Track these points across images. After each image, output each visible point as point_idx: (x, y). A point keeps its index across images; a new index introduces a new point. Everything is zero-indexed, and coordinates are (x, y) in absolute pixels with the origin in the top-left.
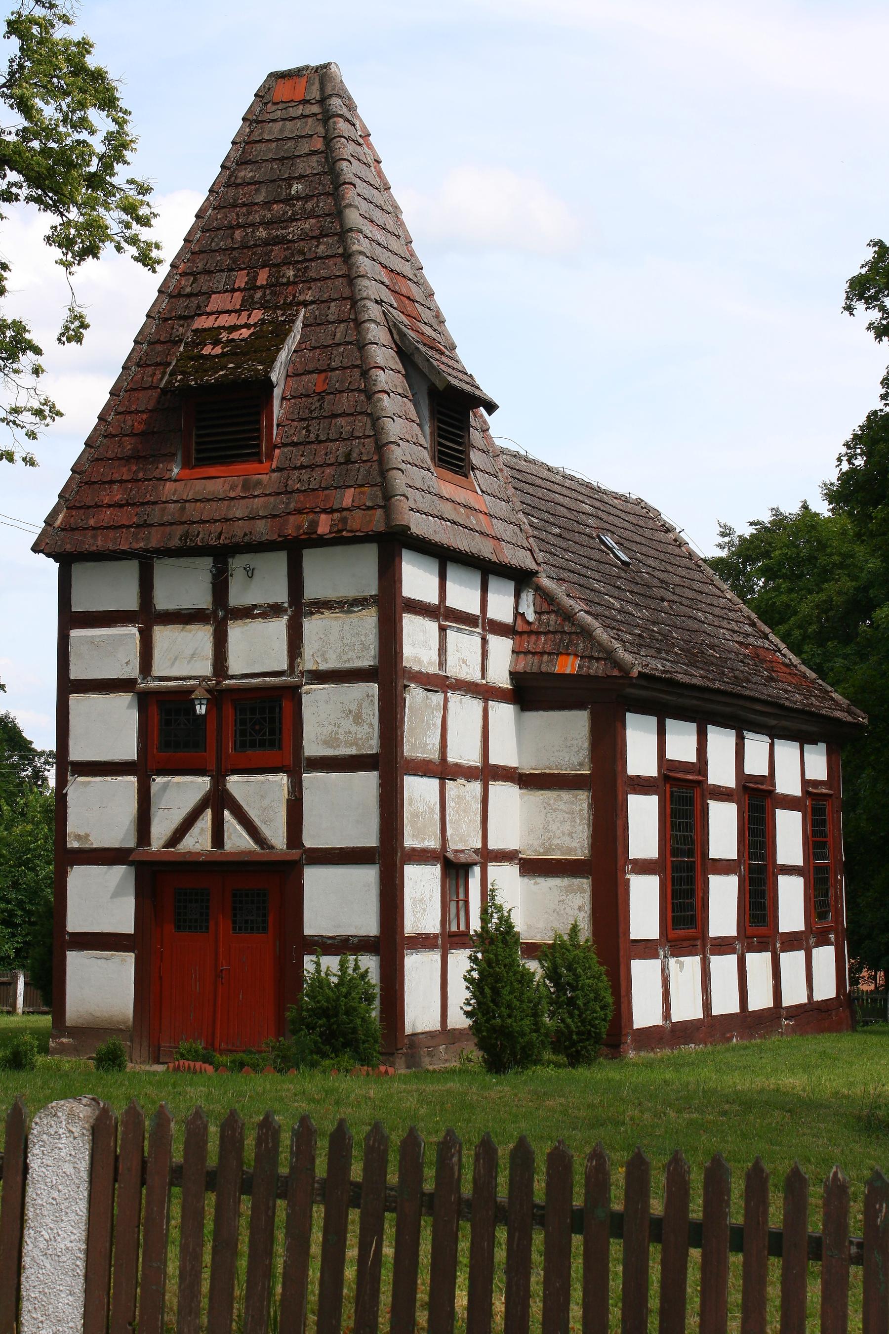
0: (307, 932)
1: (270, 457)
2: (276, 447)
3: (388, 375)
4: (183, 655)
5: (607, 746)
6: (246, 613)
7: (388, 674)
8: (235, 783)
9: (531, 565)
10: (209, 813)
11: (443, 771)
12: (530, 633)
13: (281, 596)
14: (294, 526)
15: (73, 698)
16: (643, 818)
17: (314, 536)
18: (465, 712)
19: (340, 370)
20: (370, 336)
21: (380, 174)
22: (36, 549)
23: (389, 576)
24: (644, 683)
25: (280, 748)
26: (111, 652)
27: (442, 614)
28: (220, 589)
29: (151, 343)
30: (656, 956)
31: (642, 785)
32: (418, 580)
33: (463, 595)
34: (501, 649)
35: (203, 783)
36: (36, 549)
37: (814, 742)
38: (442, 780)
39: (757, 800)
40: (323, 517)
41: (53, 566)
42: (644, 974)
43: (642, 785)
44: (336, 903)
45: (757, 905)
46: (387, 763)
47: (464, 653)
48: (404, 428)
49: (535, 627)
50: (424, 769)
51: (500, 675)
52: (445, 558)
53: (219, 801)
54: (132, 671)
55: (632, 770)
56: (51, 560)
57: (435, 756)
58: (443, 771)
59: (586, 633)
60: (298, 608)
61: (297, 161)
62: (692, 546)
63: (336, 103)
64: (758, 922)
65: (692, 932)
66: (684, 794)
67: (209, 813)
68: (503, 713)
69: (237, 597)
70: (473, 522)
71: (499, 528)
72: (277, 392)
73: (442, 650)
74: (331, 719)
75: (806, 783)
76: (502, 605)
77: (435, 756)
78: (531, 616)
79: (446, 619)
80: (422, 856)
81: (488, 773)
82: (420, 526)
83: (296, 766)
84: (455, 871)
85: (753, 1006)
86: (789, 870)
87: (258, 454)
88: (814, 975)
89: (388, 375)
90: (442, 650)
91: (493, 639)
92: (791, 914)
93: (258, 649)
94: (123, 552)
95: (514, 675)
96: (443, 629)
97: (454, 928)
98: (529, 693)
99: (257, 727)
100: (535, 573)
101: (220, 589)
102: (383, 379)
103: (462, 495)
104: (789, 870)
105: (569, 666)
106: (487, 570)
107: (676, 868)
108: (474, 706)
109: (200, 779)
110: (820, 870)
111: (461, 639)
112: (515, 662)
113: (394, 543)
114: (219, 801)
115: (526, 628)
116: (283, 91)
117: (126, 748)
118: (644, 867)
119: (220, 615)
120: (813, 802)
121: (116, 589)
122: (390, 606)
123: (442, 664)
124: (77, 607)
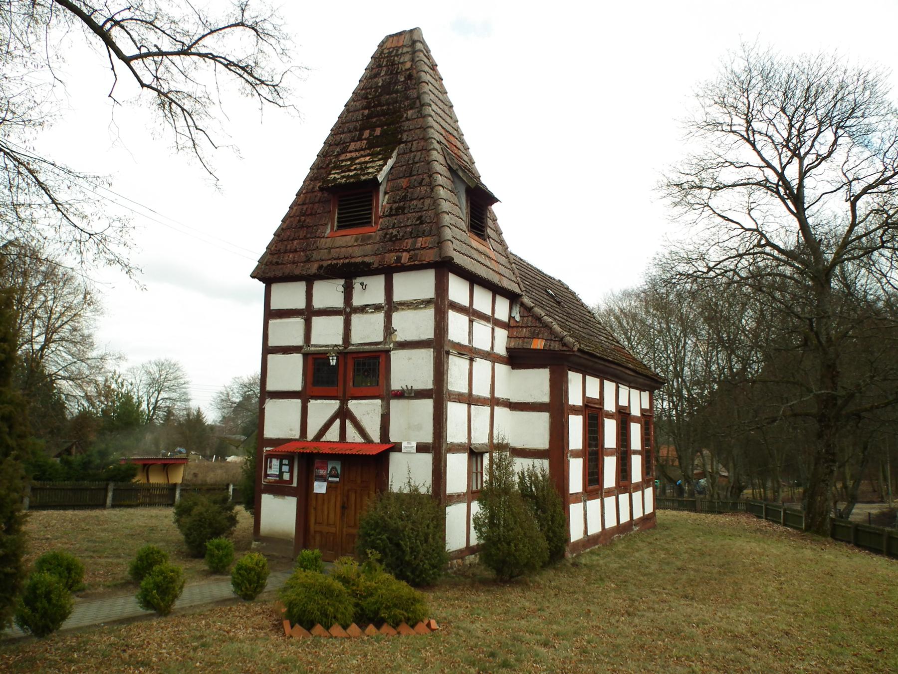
1: (376, 223)
2: (380, 217)
3: (442, 178)
4: (327, 333)
5: (558, 388)
6: (363, 309)
7: (439, 346)
8: (353, 405)
9: (517, 290)
10: (338, 421)
11: (470, 400)
12: (518, 327)
13: (380, 299)
14: (391, 258)
15: (270, 356)
16: (576, 425)
18: (482, 367)
19: (415, 180)
20: (433, 158)
21: (442, 85)
22: (253, 276)
23: (441, 288)
24: (579, 354)
26: (290, 332)
27: (472, 313)
29: (318, 169)
30: (580, 501)
31: (575, 410)
32: (458, 290)
33: (482, 301)
34: (502, 335)
35: (335, 405)
36: (253, 276)
37: (644, 391)
38: (469, 405)
39: (623, 416)
40: (405, 254)
41: (262, 286)
42: (575, 510)
43: (575, 410)
44: (408, 472)
45: (624, 470)
46: (438, 394)
47: (483, 336)
48: (453, 210)
49: (520, 324)
50: (460, 398)
51: (501, 349)
52: (473, 280)
53: (344, 414)
55: (571, 402)
56: (256, 280)
57: (465, 390)
58: (470, 400)
59: (547, 326)
60: (390, 307)
61: (395, 97)
62: (583, 301)
63: (419, 46)
64: (624, 482)
65: (596, 487)
66: (593, 413)
67: (338, 421)
68: (502, 369)
69: (357, 301)
70: (489, 264)
71: (502, 270)
72: (382, 189)
73: (470, 333)
74: (410, 369)
75: (642, 410)
76: (503, 310)
77: (465, 390)
78: (518, 318)
79: (473, 315)
80: (457, 448)
81: (493, 402)
82: (459, 259)
83: (388, 396)
84: (474, 454)
86: (635, 452)
87: (370, 222)
88: (643, 503)
89: (442, 178)
90: (470, 333)
91: (497, 329)
92: (637, 475)
93: (367, 330)
94: (297, 276)
95: (508, 349)
96: (471, 321)
97: (474, 488)
98: (517, 359)
100: (520, 296)
102: (440, 180)
103: (481, 248)
104: (635, 452)
105: (538, 344)
106: (496, 290)
107: (590, 454)
108: (487, 364)
109: (333, 402)
110: (647, 451)
111: (480, 326)
112: (508, 342)
113: (444, 267)
114: (344, 414)
115: (515, 324)
116: (388, 45)
117: (296, 383)
118: (576, 454)
119: (348, 311)
120: (646, 418)
121: (290, 296)
122: (441, 304)
123: (470, 341)
124: (274, 306)
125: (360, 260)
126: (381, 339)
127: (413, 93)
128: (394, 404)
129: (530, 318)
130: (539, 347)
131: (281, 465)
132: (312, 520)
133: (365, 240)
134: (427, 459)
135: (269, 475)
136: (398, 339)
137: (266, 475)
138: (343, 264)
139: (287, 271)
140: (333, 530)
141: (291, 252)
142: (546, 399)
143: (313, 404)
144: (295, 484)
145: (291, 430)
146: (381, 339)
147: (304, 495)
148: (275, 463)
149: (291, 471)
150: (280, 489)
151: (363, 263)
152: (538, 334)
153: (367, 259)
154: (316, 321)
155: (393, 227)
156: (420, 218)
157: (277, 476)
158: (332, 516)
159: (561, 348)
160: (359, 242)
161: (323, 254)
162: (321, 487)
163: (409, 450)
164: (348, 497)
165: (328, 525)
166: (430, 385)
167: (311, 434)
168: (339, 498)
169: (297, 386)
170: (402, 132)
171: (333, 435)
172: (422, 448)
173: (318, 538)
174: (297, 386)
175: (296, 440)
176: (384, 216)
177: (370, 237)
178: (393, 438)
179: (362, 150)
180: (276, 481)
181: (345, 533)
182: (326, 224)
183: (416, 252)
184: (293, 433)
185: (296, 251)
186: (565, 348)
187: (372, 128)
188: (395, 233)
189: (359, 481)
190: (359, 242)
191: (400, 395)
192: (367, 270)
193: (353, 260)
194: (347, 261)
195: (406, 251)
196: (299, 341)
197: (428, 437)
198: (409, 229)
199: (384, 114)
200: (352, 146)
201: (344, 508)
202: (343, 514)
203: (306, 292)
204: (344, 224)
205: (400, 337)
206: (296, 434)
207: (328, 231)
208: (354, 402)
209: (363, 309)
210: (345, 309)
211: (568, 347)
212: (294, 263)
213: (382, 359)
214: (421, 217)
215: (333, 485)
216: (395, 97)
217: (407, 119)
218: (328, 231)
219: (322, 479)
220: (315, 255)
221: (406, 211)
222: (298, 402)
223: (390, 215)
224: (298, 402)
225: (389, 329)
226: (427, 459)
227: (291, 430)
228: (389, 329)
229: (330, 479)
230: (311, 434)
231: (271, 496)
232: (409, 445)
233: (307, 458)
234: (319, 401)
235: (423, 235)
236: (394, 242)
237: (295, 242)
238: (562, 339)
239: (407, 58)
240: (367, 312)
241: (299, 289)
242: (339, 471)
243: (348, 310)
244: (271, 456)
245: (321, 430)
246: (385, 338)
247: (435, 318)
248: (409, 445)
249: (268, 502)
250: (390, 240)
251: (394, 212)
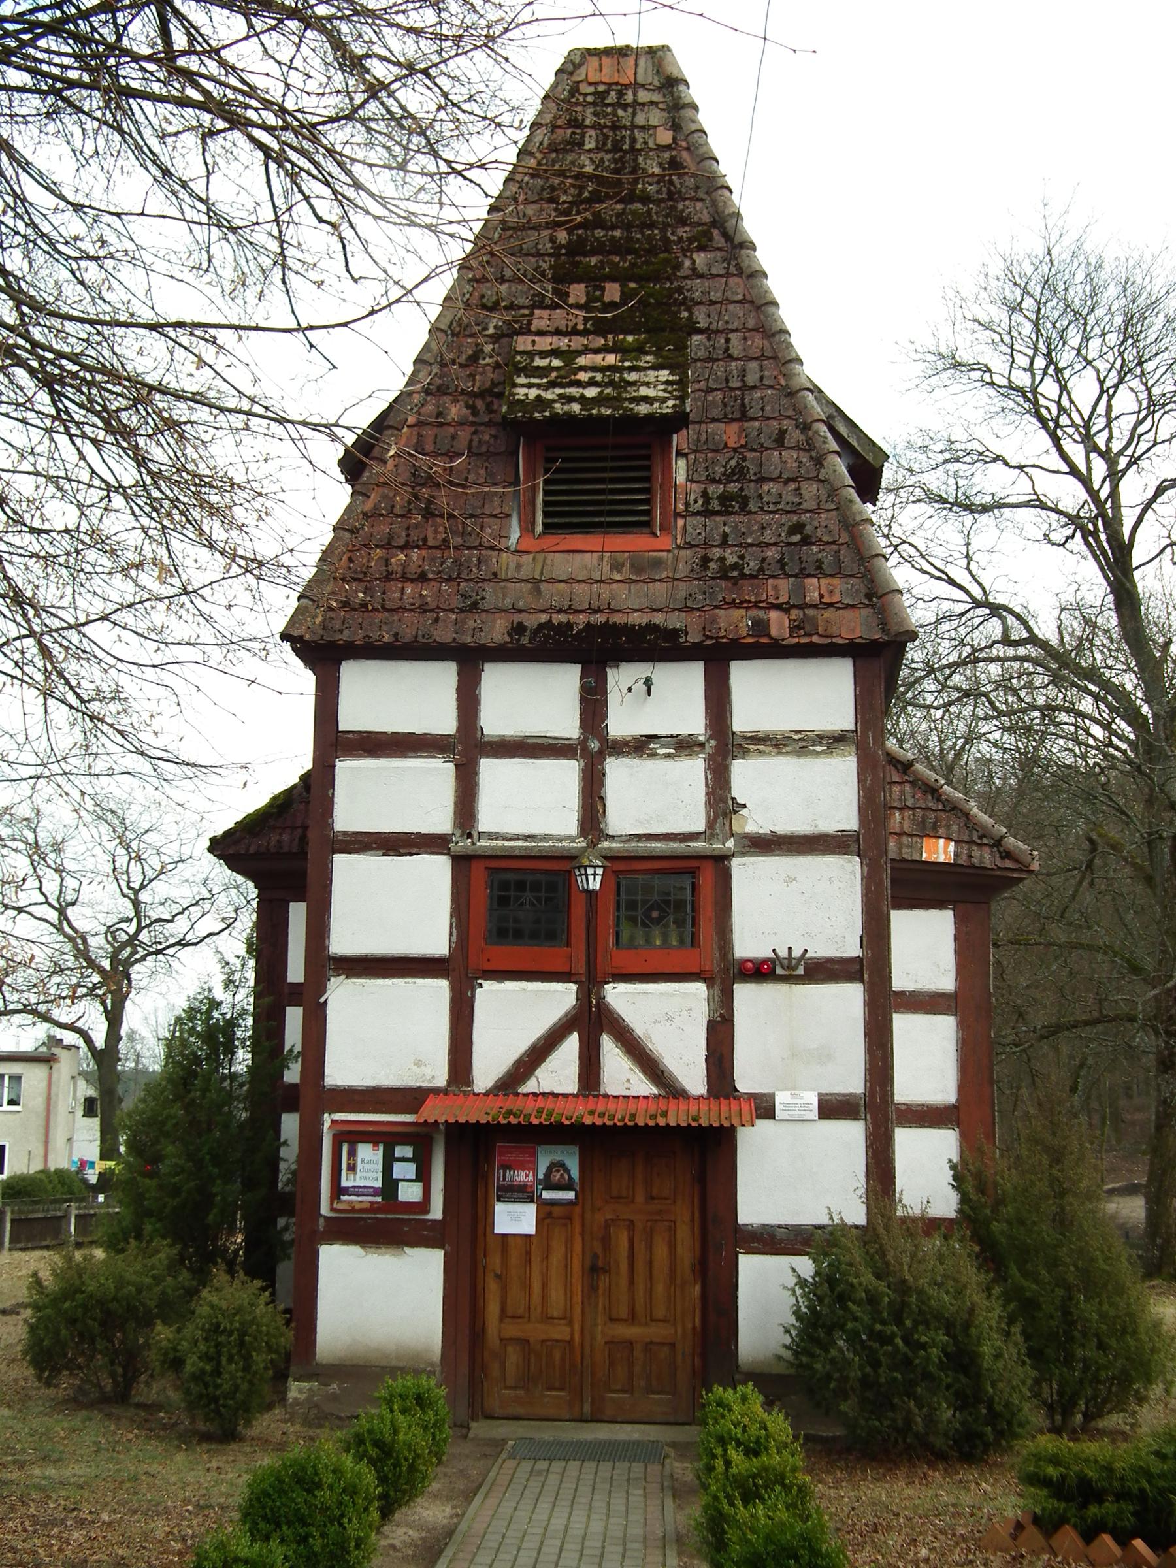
0: (742, 1220)
1: (666, 528)
2: (677, 515)
4: (529, 804)
6: (640, 746)
10: (572, 1043)
13: (695, 723)
14: (736, 622)
17: (765, 640)
25: (568, 945)
28: (593, 706)
35: (560, 998)
53: (592, 1022)
54: (441, 821)
67: (572, 1043)
85: (410, 1155)
87: (647, 524)
93: (655, 801)
99: (655, 914)
101: (593, 706)
105: (941, 851)
114: (592, 1022)
116: (590, 70)
125: (637, 619)
126: (699, 826)
127: (700, 212)
128: (745, 994)
129: (908, 787)
130: (942, 859)
131: (389, 1161)
132: (493, 1309)
133: (644, 569)
134: (851, 1135)
135: (346, 1191)
136: (751, 828)
137: (338, 1191)
138: (588, 625)
139: (407, 634)
140: (560, 1332)
141: (405, 578)
142: (946, 982)
143: (491, 996)
144: (436, 1212)
145: (418, 1063)
146: (699, 826)
147: (463, 1238)
148: (369, 1156)
149: (423, 1176)
150: (383, 1226)
151: (652, 628)
152: (935, 827)
153: (658, 619)
154: (490, 769)
155: (724, 542)
156: (797, 528)
157: (376, 1192)
158: (557, 1295)
159: (999, 863)
160: (626, 573)
161: (518, 593)
162: (516, 1218)
163: (796, 1114)
164: (606, 1242)
165: (547, 1318)
166: (852, 948)
167: (487, 1069)
168: (578, 1247)
169: (435, 939)
170: (690, 304)
171: (560, 1073)
172: (833, 1108)
173: (513, 1357)
174: (435, 939)
175: (436, 1091)
176: (688, 513)
177: (657, 564)
178: (746, 1080)
179: (574, 332)
180: (373, 1208)
181: (600, 1340)
182: (508, 516)
183: (810, 612)
184: (428, 1071)
185: (422, 578)
186: (1008, 864)
187: (595, 280)
188: (731, 559)
189: (640, 1198)
190: (626, 573)
191: (761, 971)
192: (656, 646)
193: (618, 619)
194: (601, 618)
195: (777, 607)
196: (441, 821)
197: (851, 1080)
198: (770, 553)
199: (616, 248)
200: (541, 319)
201: (594, 1270)
202: (591, 1289)
203: (459, 690)
204: (566, 518)
205: (754, 822)
206: (437, 1074)
207: (515, 534)
208: (622, 987)
209: (640, 746)
210: (583, 743)
211: (1017, 861)
212: (424, 609)
213: (707, 878)
214: (803, 526)
215: (557, 1211)
216: (620, 214)
217: (695, 273)
218: (515, 534)
219: (522, 1194)
220: (491, 595)
221: (752, 506)
222: (439, 989)
223: (707, 513)
224: (439, 989)
225: (721, 802)
226: (851, 1135)
227: (418, 1063)
228: (721, 802)
229: (546, 1195)
230: (487, 1069)
231: (356, 1250)
232: (797, 1100)
233: (475, 1142)
234: (510, 985)
235: (819, 570)
236: (735, 581)
237: (415, 554)
238: (998, 842)
239: (655, 117)
240: (653, 755)
241: (564, 681)
242: (575, 1173)
243: (594, 745)
244: (350, 1137)
245: (518, 1063)
246: (710, 824)
247: (861, 780)
248: (797, 1100)
249: (342, 1270)
250: (725, 577)
251: (715, 505)
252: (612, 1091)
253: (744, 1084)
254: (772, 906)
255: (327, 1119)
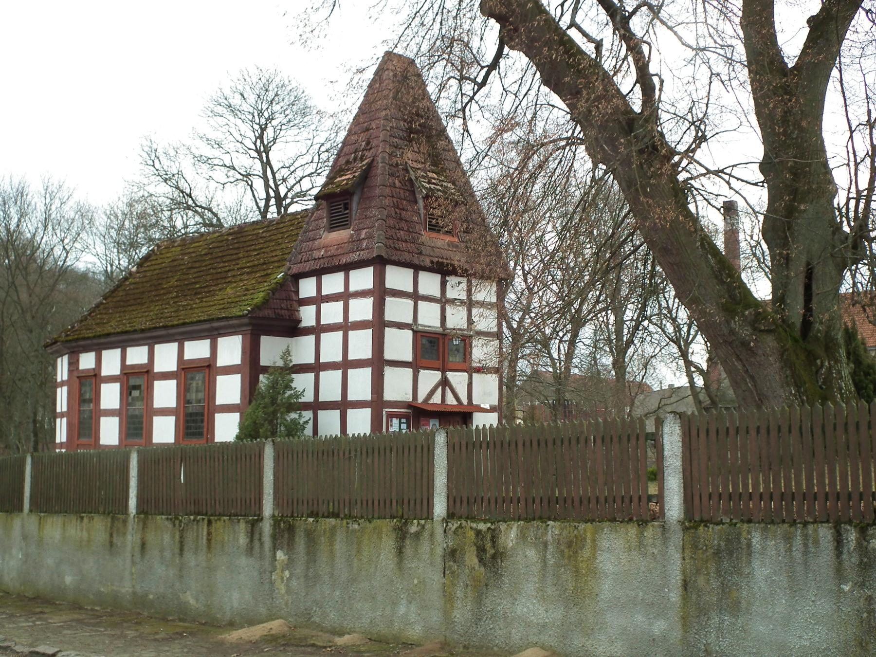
4: (429, 316)
10: (440, 389)
35: (437, 376)
53: (445, 383)
131: (400, 423)
143: (423, 373)
145: (360, 71)
146: (466, 327)
148: (395, 421)
154: (351, 397)
167: (421, 398)
169: (408, 357)
174: (408, 357)
222: (409, 371)
224: (409, 371)
230: (421, 398)
244: (391, 416)
252: (449, 403)
253: (474, 403)
254: (481, 352)
255: (385, 410)
